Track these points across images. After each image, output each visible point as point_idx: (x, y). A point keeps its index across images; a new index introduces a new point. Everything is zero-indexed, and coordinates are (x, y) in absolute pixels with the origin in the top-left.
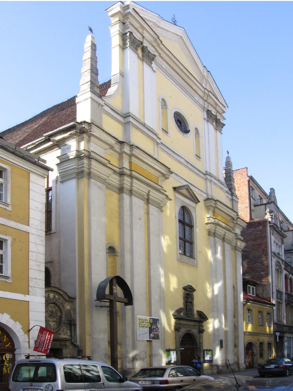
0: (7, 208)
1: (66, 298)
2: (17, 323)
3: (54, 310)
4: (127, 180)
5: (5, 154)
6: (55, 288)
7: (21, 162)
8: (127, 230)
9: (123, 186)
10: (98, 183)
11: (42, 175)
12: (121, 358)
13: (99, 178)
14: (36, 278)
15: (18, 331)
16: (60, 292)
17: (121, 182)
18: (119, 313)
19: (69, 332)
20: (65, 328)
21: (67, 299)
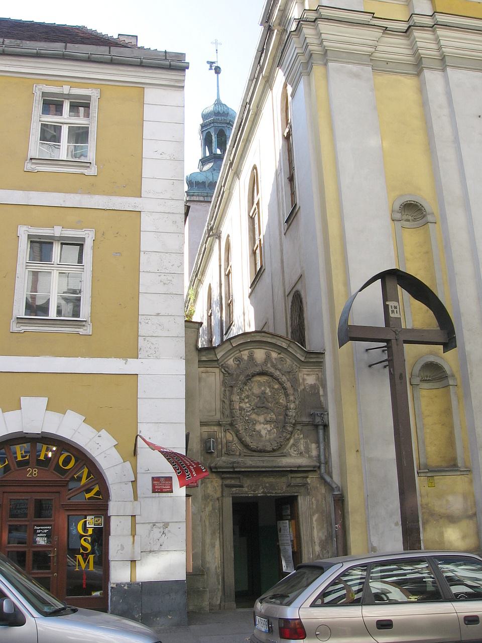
0: (86, 172)
1: (298, 356)
2: (103, 432)
3: (268, 390)
4: (423, 39)
5: (79, 69)
6: (263, 334)
7: (117, 73)
8: (445, 152)
9: (420, 54)
10: (350, 66)
11: (172, 83)
12: (475, 514)
13: (350, 57)
14: (158, 315)
15: (103, 455)
16: (279, 343)
17: (413, 46)
18: (453, 376)
19: (314, 446)
20: (302, 436)
21: (303, 359)
